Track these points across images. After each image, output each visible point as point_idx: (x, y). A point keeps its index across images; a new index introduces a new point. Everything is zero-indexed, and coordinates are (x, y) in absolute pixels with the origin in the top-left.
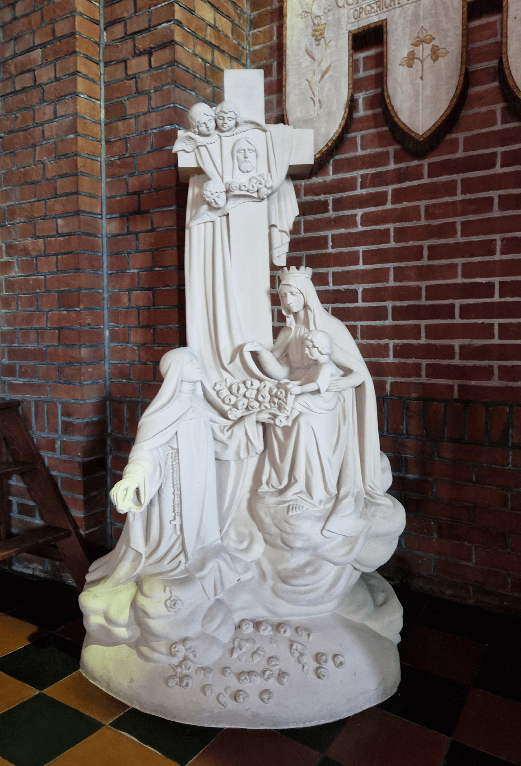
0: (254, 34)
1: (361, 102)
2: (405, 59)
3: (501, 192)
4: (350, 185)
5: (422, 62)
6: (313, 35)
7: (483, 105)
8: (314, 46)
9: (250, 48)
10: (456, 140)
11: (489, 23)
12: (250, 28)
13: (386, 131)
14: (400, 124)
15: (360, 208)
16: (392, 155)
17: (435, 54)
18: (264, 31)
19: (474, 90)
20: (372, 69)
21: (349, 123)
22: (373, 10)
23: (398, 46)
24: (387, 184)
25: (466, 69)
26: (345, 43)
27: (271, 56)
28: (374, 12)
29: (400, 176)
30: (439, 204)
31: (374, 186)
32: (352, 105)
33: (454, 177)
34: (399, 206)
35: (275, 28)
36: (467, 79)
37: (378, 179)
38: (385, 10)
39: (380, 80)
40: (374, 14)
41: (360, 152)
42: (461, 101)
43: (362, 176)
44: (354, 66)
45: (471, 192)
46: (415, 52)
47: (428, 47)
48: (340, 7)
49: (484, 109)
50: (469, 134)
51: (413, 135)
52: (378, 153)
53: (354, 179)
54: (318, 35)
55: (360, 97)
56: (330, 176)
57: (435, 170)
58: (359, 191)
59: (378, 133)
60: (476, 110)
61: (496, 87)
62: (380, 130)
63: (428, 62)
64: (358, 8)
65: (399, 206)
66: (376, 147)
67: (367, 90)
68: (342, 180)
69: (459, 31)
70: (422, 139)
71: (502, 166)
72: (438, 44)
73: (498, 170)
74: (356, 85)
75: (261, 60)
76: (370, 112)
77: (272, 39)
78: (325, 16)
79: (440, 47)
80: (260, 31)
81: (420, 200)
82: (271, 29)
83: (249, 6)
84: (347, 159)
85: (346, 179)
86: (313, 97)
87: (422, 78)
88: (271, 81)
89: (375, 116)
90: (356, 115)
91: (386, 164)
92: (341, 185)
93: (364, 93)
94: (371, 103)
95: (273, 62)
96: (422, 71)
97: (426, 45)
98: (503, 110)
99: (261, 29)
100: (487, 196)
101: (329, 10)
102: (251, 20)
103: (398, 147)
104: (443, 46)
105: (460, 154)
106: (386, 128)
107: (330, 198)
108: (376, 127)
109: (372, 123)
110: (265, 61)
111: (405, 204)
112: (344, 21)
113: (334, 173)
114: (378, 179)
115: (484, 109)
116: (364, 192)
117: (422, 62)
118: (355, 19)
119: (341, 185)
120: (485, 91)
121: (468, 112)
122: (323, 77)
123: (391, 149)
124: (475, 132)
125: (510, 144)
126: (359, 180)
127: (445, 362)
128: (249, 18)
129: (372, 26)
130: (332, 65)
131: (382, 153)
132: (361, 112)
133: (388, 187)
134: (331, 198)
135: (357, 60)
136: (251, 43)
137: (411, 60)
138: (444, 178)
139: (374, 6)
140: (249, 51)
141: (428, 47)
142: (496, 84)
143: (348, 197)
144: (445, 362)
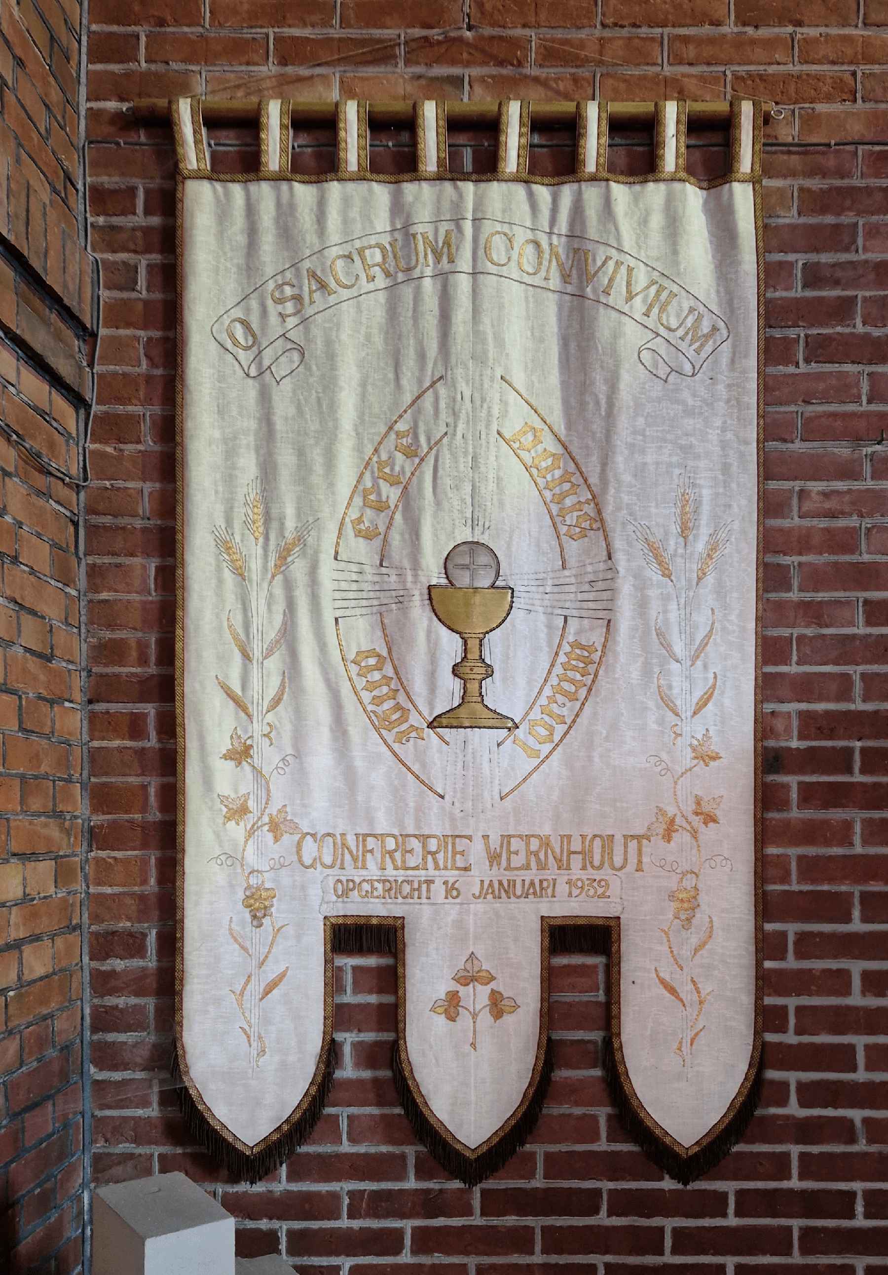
0: (98, 861)
1: (347, 1050)
2: (440, 1003)
3: (609, 1258)
4: (326, 1207)
5: (475, 1016)
6: (247, 907)
7: (577, 1104)
8: (249, 928)
9: (88, 887)
10: (533, 1155)
11: (584, 966)
12: (90, 846)
13: (399, 1115)
14: (432, 1120)
15: (347, 1255)
16: (411, 1161)
17: (498, 1006)
18: (126, 861)
19: (562, 1074)
20: (370, 992)
21: (324, 1088)
22: (375, 894)
23: (427, 976)
24: (403, 1216)
25: (549, 1040)
26: (316, 942)
27: (142, 915)
28: (377, 897)
29: (429, 1204)
30: (502, 1265)
31: (377, 1216)
32: (331, 1053)
33: (529, 1221)
34: (426, 1260)
35: (153, 861)
36: (550, 1055)
37: (381, 1204)
38: (400, 900)
39: (391, 1017)
40: (377, 900)
41: (346, 1147)
42: (541, 1089)
43: (351, 1194)
44: (333, 982)
45: (559, 1252)
46: (460, 994)
47: (483, 992)
48: (307, 867)
49: (578, 1111)
50: (554, 1148)
51: (458, 1147)
52: (382, 1154)
53: (335, 1197)
54: (257, 906)
55: (348, 1039)
56: (281, 1183)
57: (494, 1203)
58: (344, 1223)
59: (383, 1116)
60: (565, 1109)
61: (598, 1077)
62: (387, 1111)
63: (485, 1018)
64: (344, 879)
65: (426, 1260)
66: (379, 1143)
67: (360, 1031)
68: (308, 1197)
69: (537, 971)
70: (473, 1156)
71: (610, 1214)
72: (501, 989)
73: (603, 1219)
74: (338, 1016)
75: (119, 919)
76: (367, 1074)
77: (145, 882)
78: (272, 873)
79: (505, 995)
80: (115, 858)
81: (467, 1253)
82: (145, 862)
83: (87, 802)
84: (319, 1156)
85: (318, 1194)
86: (247, 1027)
87: (473, 1045)
88: (144, 969)
89: (376, 1082)
90: (339, 1074)
91: (401, 1177)
92: (307, 1206)
93: (353, 1035)
94: (369, 1056)
95: (149, 928)
96: (475, 1034)
97: (479, 987)
98: (610, 1118)
99: (119, 854)
100: (585, 1262)
101: (283, 866)
102: (91, 830)
103: (421, 1148)
104: (510, 994)
105: (538, 1182)
106: (398, 1110)
107: (283, 1227)
108: (379, 1104)
109: (372, 1096)
110: (129, 924)
111: (439, 1258)
112: (315, 893)
113: (290, 1179)
114: (381, 1204)
115: (578, 1111)
116: (356, 1224)
117: (475, 1016)
118: (338, 897)
119: (307, 1206)
120: (581, 1081)
121: (553, 1110)
122: (267, 992)
123: (410, 1151)
124: (564, 1148)
125: (623, 1179)
126: (346, 1201)
127: (456, 1222)
128: (86, 824)
129: (374, 921)
130: (289, 973)
131: (391, 1156)
132: (348, 1071)
133: (405, 1221)
134: (285, 1228)
135: (340, 969)
136: (91, 877)
137: (451, 1006)
138: (511, 1220)
139: (379, 886)
140: (87, 893)
141: (483, 992)
142: (597, 1072)
143: (320, 1229)
144: (456, 1222)
